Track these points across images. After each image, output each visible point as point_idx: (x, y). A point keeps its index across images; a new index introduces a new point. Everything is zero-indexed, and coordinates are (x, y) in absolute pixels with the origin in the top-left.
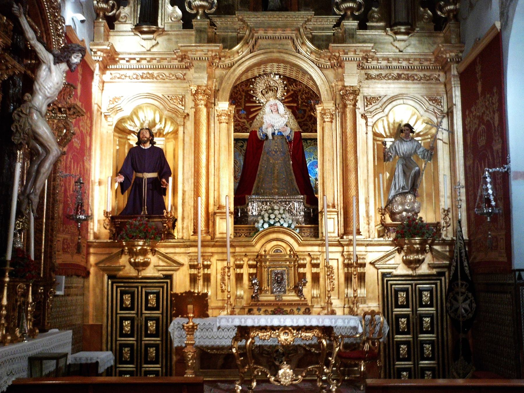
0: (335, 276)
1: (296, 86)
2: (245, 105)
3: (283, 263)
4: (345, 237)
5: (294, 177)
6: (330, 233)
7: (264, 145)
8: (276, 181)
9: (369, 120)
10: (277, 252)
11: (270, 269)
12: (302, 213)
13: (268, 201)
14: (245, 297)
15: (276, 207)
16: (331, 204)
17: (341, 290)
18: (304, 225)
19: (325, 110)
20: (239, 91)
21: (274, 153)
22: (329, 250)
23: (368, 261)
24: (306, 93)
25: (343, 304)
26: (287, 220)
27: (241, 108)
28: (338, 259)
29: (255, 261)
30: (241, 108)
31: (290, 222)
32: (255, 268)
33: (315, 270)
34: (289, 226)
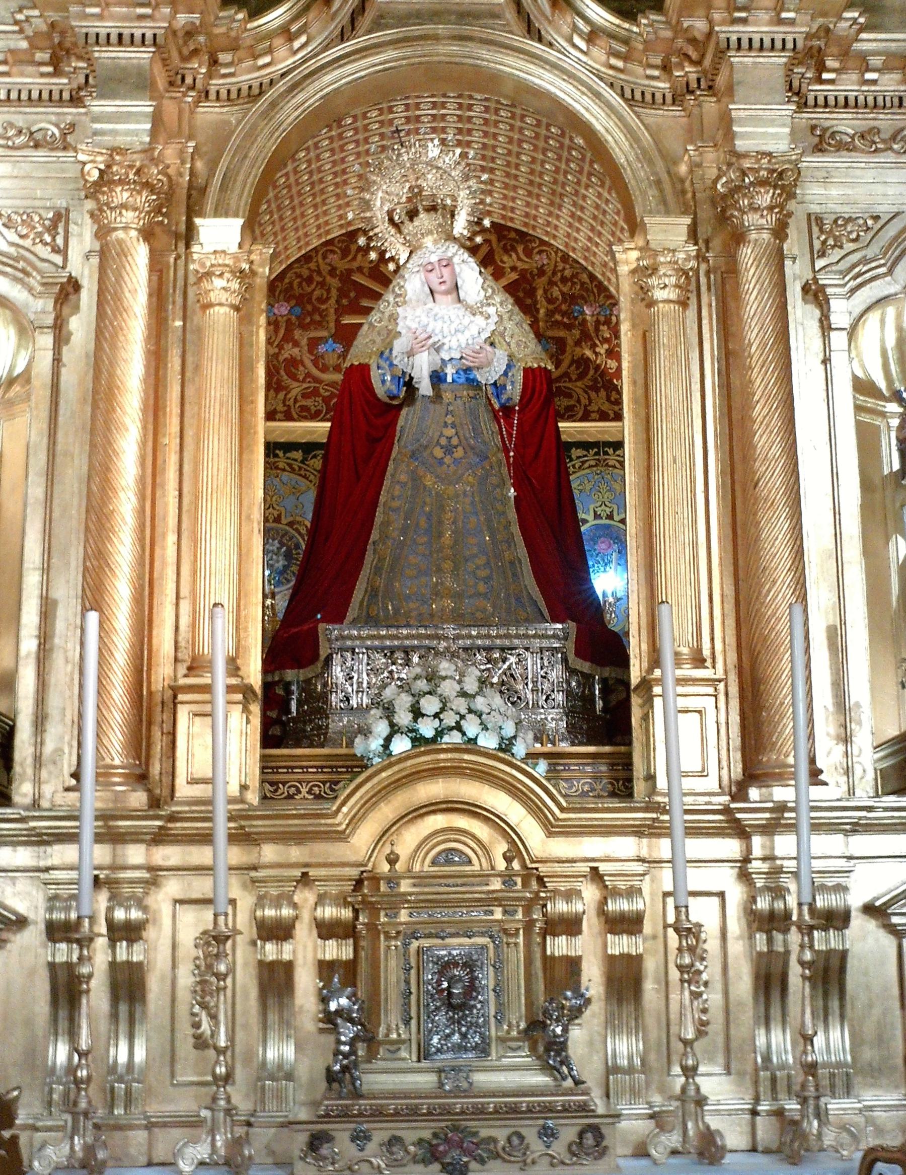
0: (711, 971)
1: (529, 253)
2: (337, 321)
3: (477, 914)
4: (754, 793)
5: (522, 551)
6: (686, 775)
7: (401, 422)
8: (447, 565)
9: (836, 305)
10: (449, 862)
11: (415, 944)
12: (560, 697)
13: (414, 649)
14: (303, 1072)
15: (445, 667)
16: (685, 650)
17: (739, 1032)
18: (565, 747)
19: (656, 253)
20: (319, 272)
21: (438, 453)
22: (690, 855)
23: (856, 900)
24: (564, 280)
25: (749, 1098)
26: (492, 720)
27: (324, 334)
28: (721, 895)
29: (346, 904)
30: (324, 334)
31: (509, 730)
32: (346, 937)
33: (621, 945)
34: (506, 746)
